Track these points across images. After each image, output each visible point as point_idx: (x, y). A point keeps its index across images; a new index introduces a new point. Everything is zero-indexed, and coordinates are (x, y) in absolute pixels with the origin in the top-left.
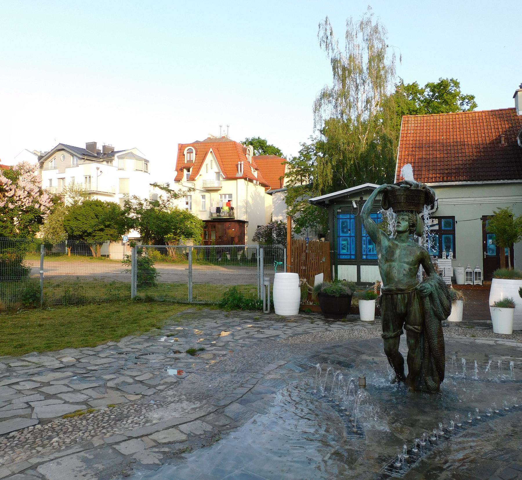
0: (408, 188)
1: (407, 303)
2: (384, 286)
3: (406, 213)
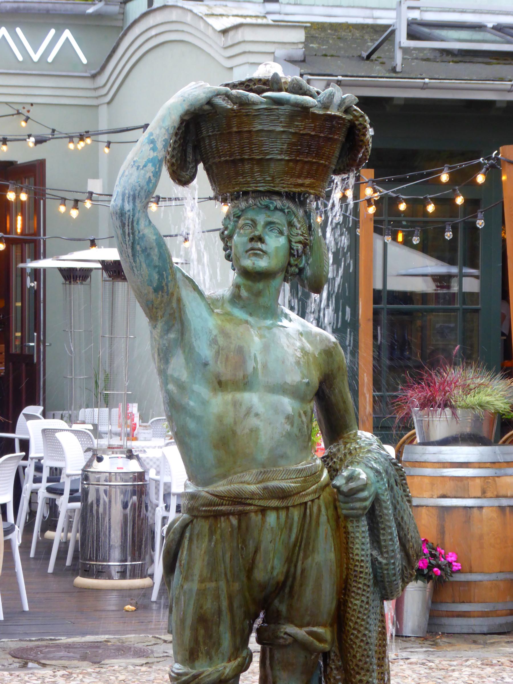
3: (278, 203)
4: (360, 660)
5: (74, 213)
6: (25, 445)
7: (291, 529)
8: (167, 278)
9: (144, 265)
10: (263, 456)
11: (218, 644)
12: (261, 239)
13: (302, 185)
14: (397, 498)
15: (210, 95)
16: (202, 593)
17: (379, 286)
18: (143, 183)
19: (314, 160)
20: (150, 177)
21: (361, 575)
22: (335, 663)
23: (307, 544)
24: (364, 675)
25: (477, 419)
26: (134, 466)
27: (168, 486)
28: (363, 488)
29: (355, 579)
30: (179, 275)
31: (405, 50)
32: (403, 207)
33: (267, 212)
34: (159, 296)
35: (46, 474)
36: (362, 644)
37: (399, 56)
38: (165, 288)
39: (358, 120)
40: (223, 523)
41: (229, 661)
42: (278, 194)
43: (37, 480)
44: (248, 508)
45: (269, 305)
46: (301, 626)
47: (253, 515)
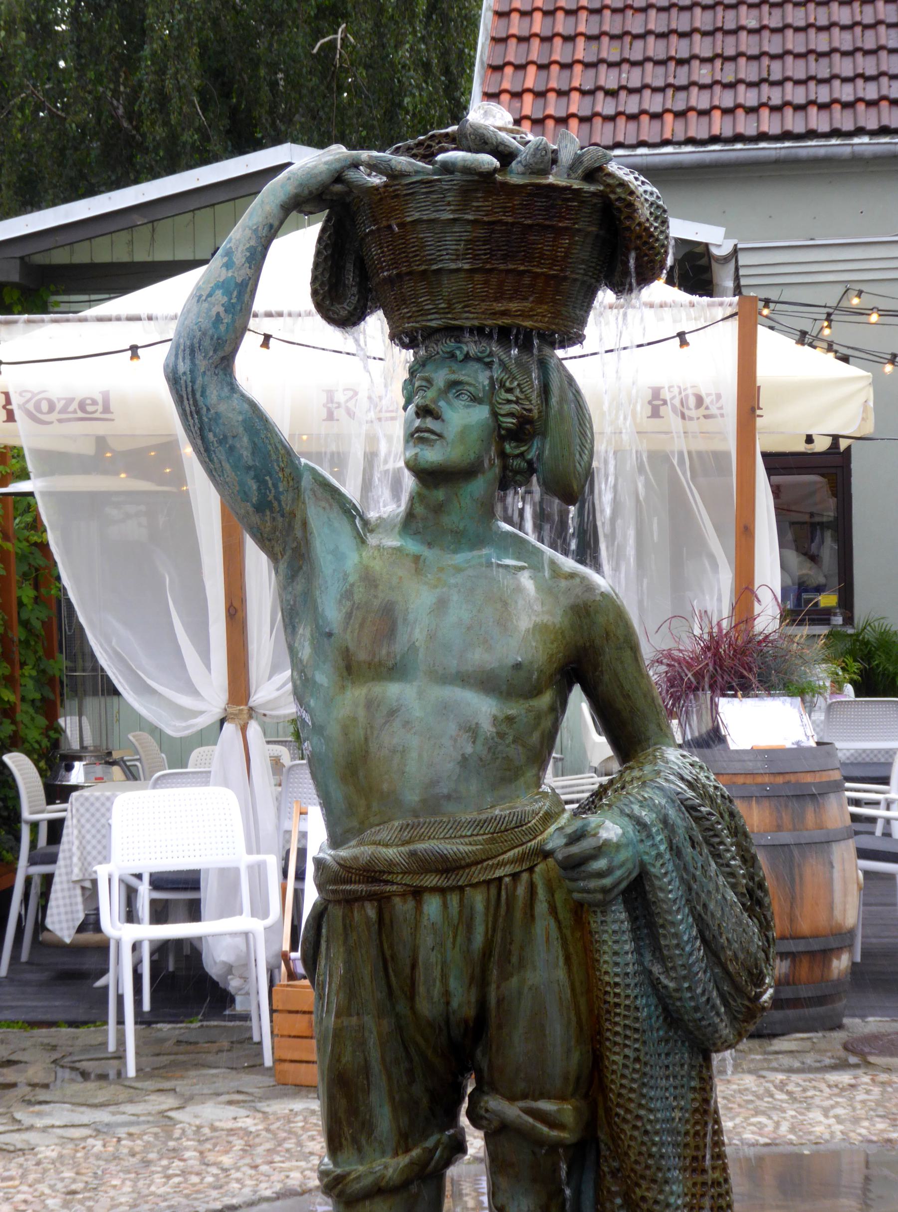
0: (487, 176)
1: (487, 953)
2: (335, 841)
3: (472, 347)
4: (637, 1162)
7: (470, 928)
8: (275, 486)
9: (227, 466)
10: (412, 797)
11: (368, 1127)
13: (504, 313)
14: (692, 869)
15: (338, 166)
18: (206, 324)
19: (522, 268)
20: (218, 314)
21: (618, 1011)
23: (506, 955)
24: (648, 1189)
29: (608, 1016)
30: (306, 482)
33: (453, 364)
34: (268, 518)
36: (636, 1133)
38: (276, 504)
39: (614, 193)
41: (396, 1154)
44: (388, 888)
45: (461, 528)
46: (512, 1098)
47: (397, 900)
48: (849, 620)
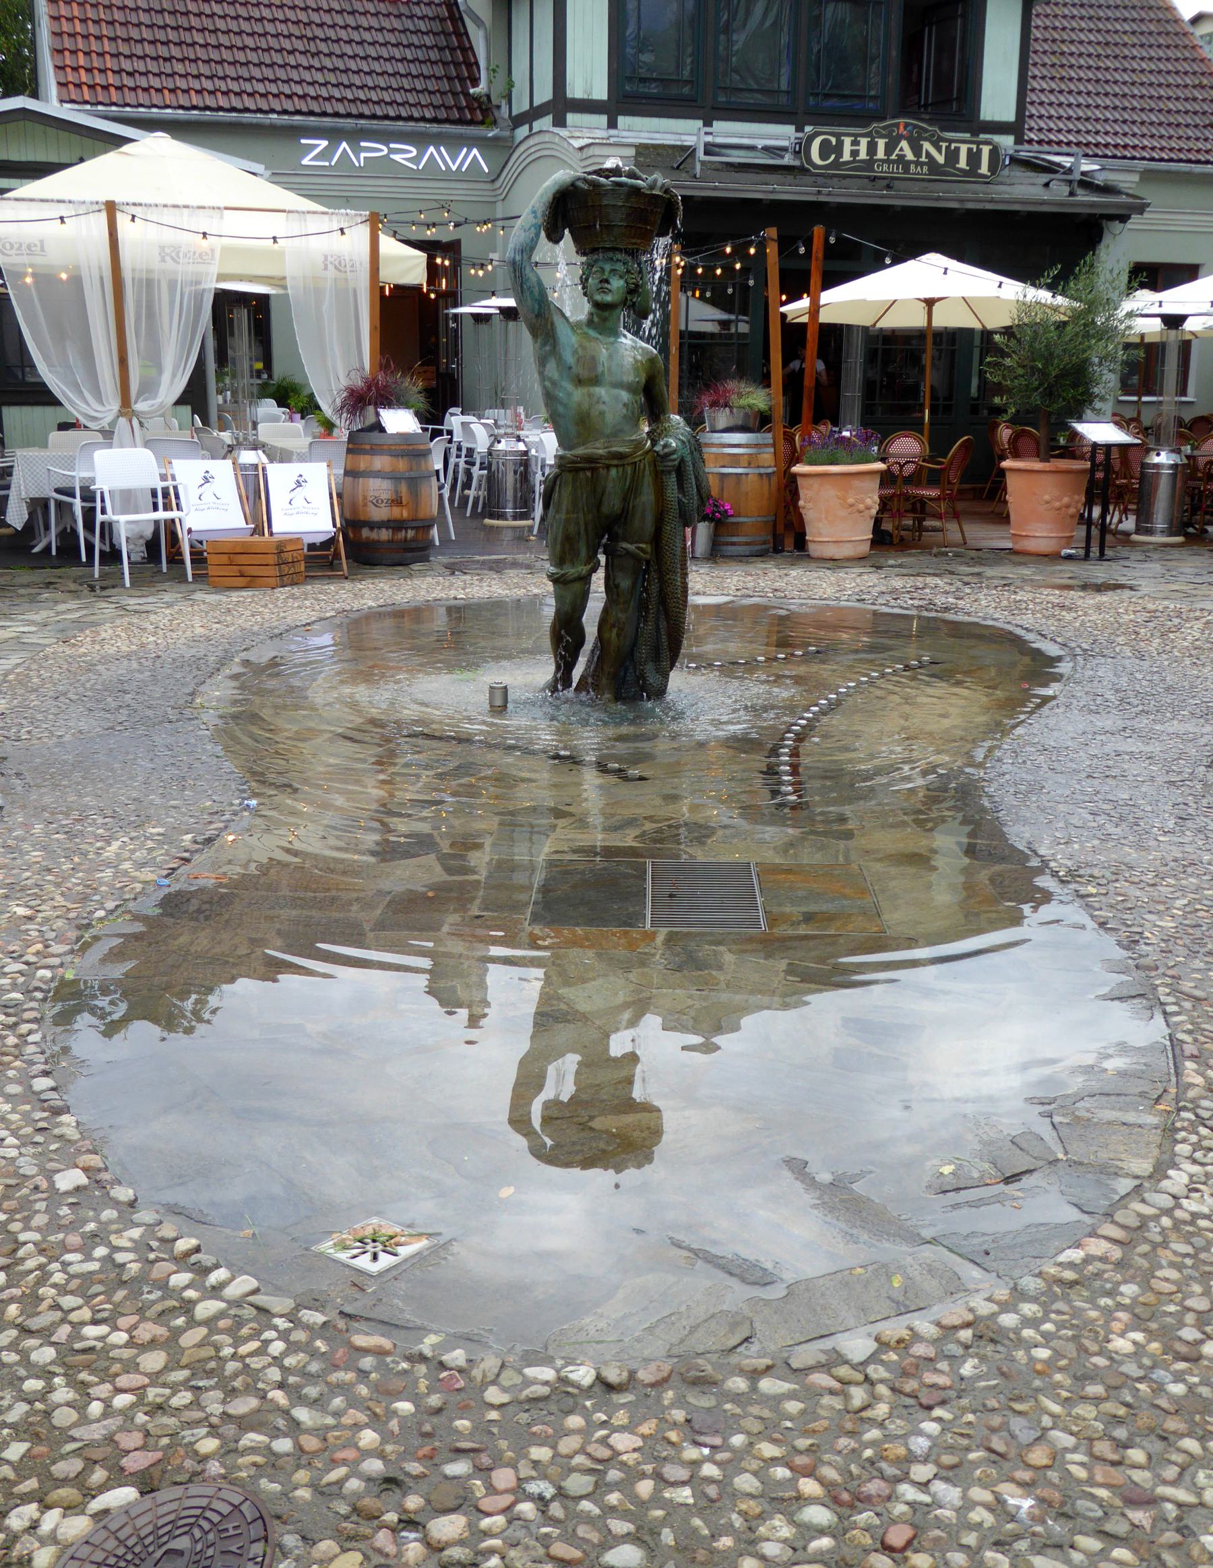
3: (619, 256)
5: (481, 273)
6: (450, 433)
10: (608, 431)
12: (607, 281)
16: (567, 521)
17: (683, 328)
22: (654, 567)
25: (746, 415)
26: (521, 447)
27: (543, 460)
28: (674, 452)
31: (703, 163)
32: (700, 271)
35: (464, 452)
37: (698, 167)
40: (581, 475)
42: (620, 250)
43: (458, 456)
48: (270, 377)
